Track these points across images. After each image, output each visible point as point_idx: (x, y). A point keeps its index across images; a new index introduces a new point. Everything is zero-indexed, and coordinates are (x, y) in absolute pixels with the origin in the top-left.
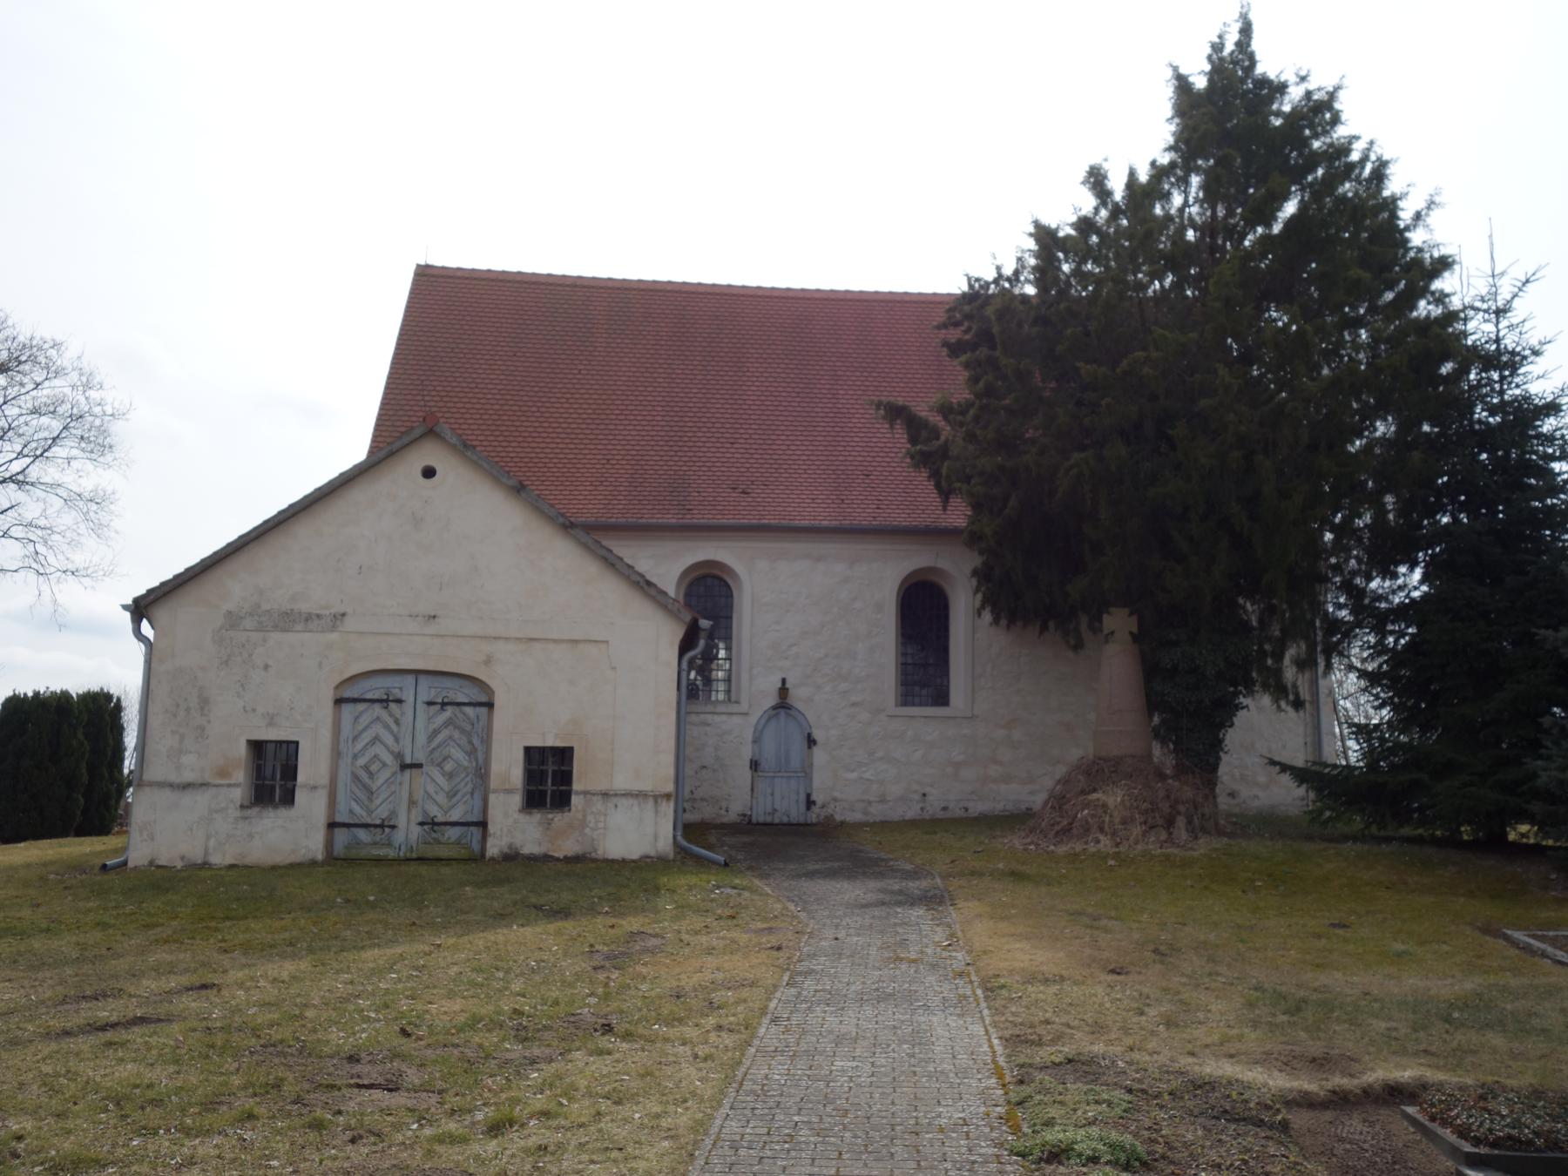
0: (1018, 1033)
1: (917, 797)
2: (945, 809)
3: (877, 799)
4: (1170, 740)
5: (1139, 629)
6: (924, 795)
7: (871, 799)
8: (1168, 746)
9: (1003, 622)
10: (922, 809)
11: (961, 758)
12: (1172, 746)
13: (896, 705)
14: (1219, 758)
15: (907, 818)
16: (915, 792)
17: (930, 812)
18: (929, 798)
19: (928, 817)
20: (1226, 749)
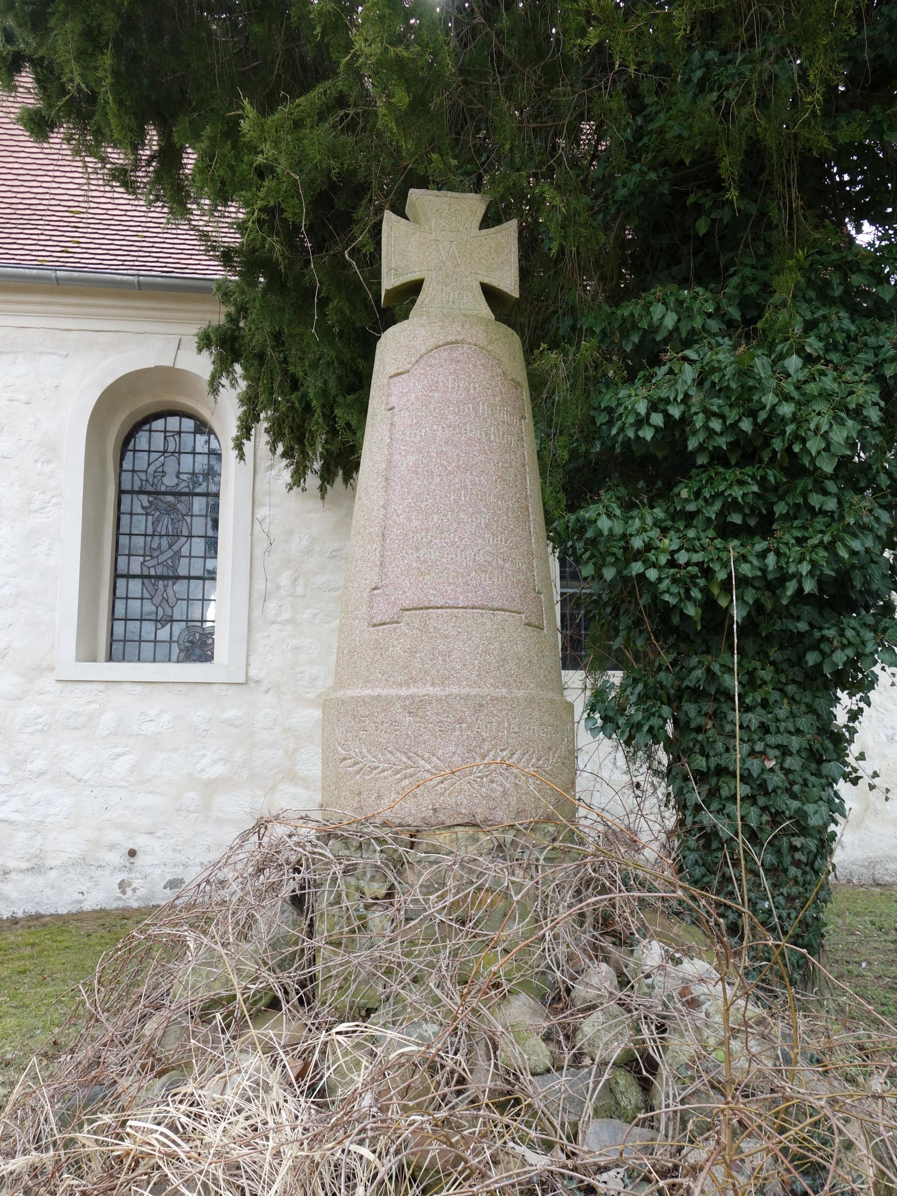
0: (573, 889)
1: (116, 858)
2: (173, 884)
3: (25, 865)
4: (655, 734)
5: (525, 274)
6: (132, 853)
7: (11, 864)
8: (650, 757)
9: (312, 481)
10: (122, 886)
11: (218, 770)
12: (663, 757)
13: (78, 660)
14: (836, 807)
15: (87, 906)
16: (112, 847)
17: (140, 893)
18: (140, 859)
19: (135, 905)
20: (865, 769)
